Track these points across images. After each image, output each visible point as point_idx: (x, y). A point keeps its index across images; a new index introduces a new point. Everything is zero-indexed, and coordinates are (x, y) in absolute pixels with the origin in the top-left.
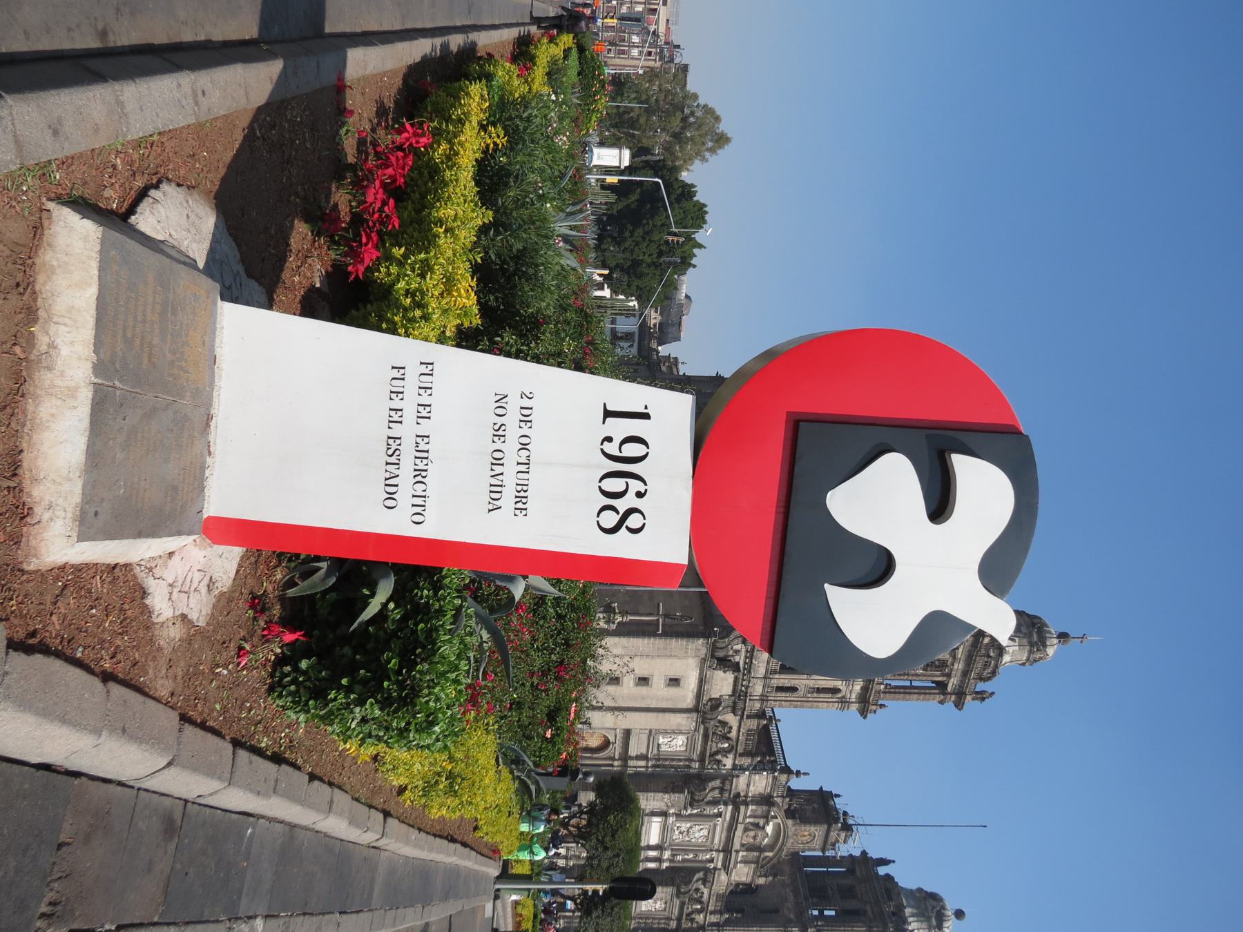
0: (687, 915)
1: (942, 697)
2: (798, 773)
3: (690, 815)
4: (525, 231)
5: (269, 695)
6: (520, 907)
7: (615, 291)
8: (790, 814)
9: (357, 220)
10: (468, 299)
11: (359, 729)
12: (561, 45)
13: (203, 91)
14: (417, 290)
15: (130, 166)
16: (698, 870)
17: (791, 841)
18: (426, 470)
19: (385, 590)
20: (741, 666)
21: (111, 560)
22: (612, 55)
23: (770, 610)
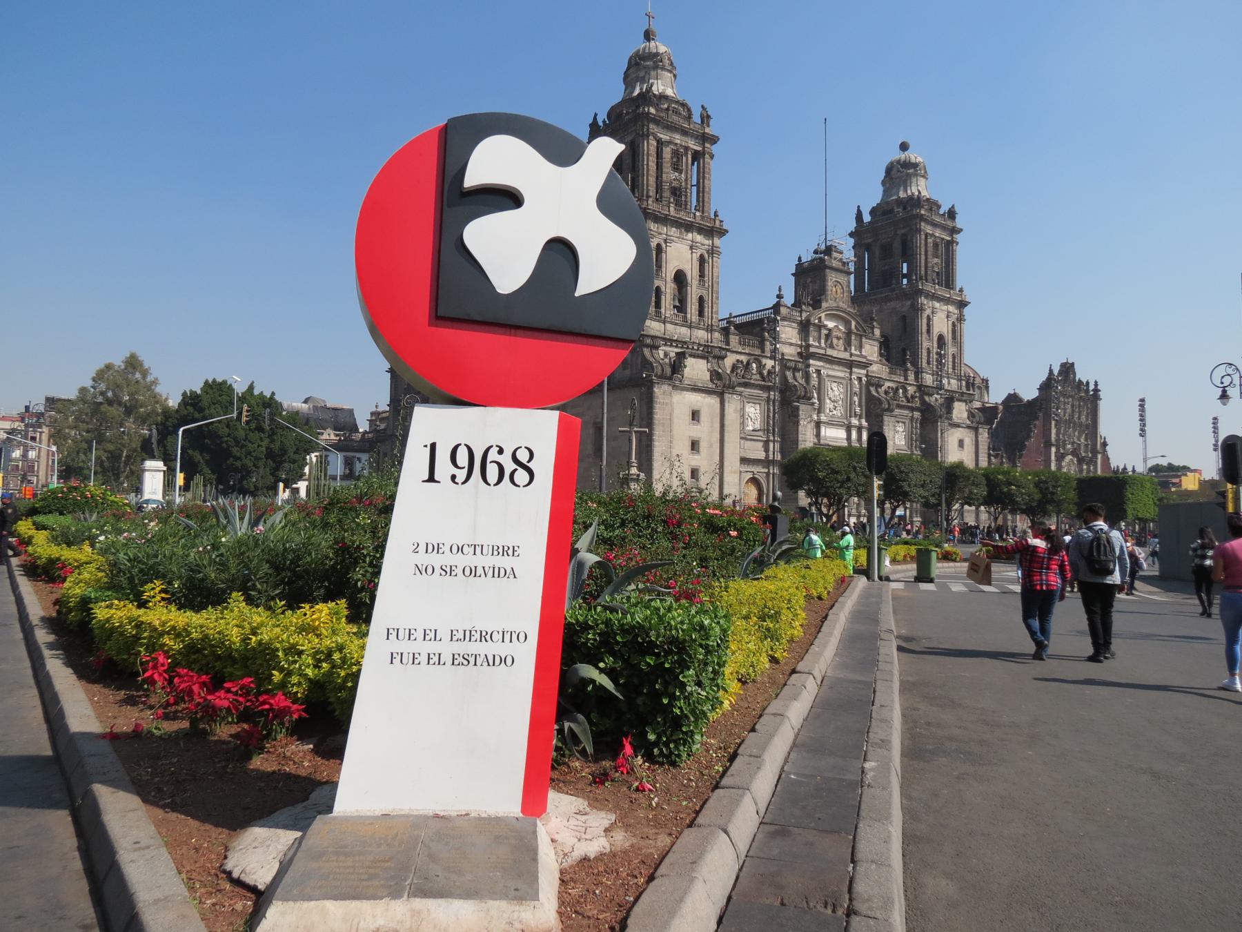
0: (908, 402)
1: (707, 156)
2: (779, 296)
3: (819, 399)
4: (251, 561)
5: (679, 766)
6: (897, 557)
7: (301, 477)
8: (816, 305)
9: (244, 716)
10: (322, 611)
11: (707, 689)
12: (31, 532)
13: (135, 843)
14: (314, 657)
15: (212, 894)
16: (869, 392)
17: (841, 303)
18: (481, 632)
19: (588, 671)
20: (679, 350)
21: (557, 882)
22: (35, 479)
23: (597, 341)
